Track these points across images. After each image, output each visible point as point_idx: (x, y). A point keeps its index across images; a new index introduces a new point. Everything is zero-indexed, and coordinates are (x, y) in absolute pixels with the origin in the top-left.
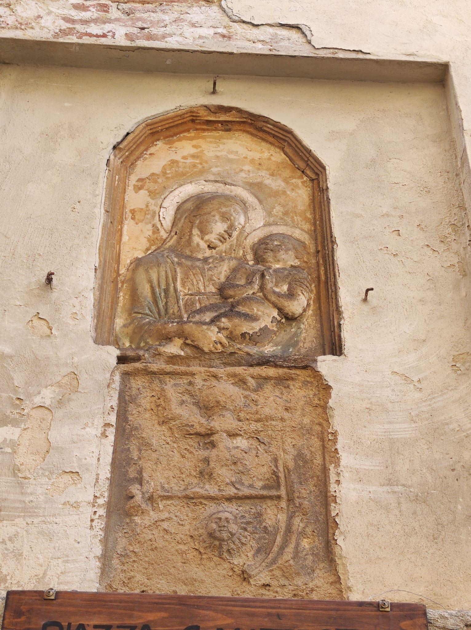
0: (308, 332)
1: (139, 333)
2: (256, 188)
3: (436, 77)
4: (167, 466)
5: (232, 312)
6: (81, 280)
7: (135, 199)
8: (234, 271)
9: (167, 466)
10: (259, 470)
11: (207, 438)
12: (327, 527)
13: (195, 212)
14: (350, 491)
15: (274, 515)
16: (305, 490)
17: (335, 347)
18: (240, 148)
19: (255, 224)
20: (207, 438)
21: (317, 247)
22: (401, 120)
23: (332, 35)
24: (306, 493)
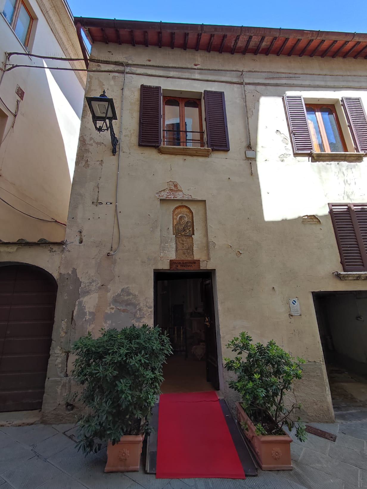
0: (191, 233)
1: (176, 233)
2: (186, 215)
3: (205, 201)
4: (180, 247)
5: (185, 231)
6: (171, 228)
7: (175, 217)
8: (286, 373)
9: (180, 247)
10: (187, 247)
11: (183, 244)
12: (193, 252)
13: (181, 218)
14: (194, 249)
15: (189, 251)
16: (191, 249)
17: (194, 234)
18: (184, 209)
19: (186, 219)
20: (183, 244)
21: (48, 14)
22: (200, 207)
23: (195, 197)
24: (191, 249)
